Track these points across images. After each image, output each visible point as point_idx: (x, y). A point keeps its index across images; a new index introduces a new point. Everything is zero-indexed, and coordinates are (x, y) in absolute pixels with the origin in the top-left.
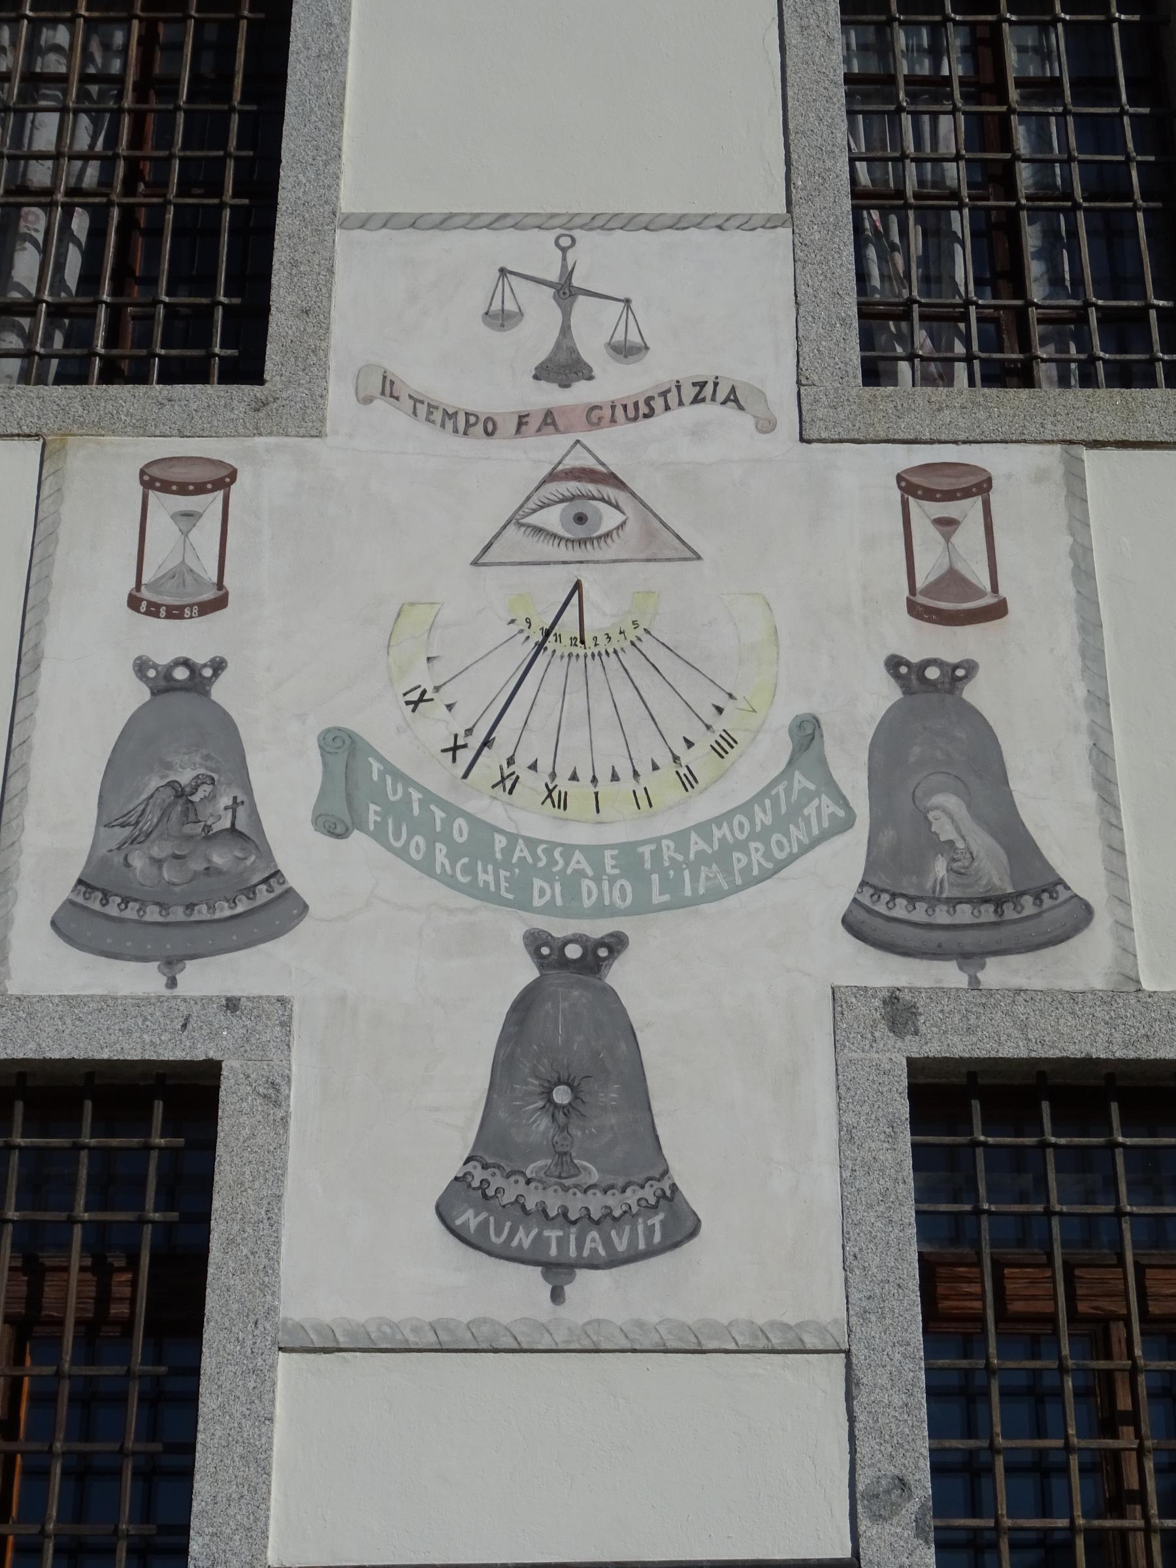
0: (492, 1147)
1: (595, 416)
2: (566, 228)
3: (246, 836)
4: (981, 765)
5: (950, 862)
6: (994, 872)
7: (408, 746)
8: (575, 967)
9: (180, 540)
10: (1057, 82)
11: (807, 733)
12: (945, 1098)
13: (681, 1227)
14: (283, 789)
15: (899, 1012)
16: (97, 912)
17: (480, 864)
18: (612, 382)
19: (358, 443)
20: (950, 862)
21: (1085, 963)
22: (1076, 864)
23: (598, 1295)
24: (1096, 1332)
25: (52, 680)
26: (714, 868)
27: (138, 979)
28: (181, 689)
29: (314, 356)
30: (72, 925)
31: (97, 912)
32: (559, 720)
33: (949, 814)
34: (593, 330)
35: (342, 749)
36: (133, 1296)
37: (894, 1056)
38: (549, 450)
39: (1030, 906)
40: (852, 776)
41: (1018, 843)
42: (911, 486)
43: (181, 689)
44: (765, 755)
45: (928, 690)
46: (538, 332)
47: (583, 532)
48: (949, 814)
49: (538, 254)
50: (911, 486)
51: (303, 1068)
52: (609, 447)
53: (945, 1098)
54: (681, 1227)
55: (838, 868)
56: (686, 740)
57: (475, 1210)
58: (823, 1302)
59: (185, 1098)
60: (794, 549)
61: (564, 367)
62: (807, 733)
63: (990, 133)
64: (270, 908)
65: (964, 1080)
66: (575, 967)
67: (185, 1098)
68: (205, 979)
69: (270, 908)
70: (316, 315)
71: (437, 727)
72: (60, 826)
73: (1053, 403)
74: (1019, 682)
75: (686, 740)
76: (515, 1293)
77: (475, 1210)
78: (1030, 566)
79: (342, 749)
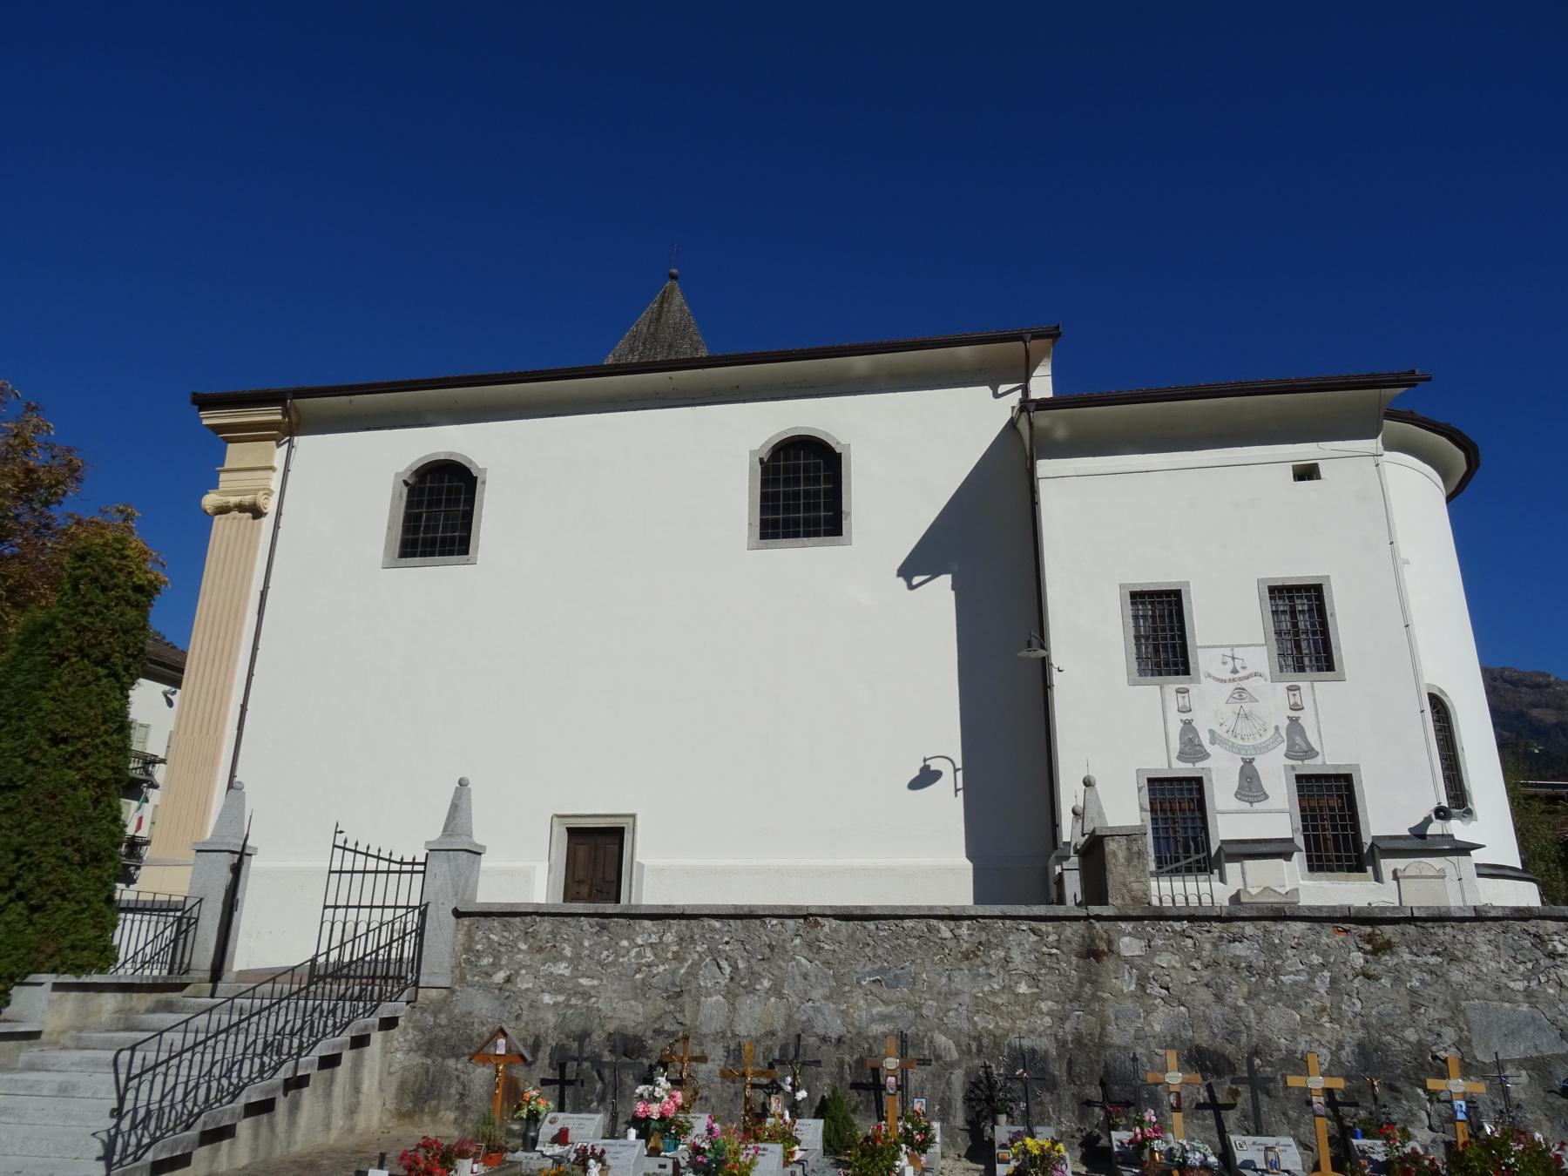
0: (1240, 787)
1: (1241, 679)
2: (1232, 647)
3: (1200, 745)
4: (1302, 732)
5: (1299, 748)
6: (1305, 747)
7: (1220, 731)
8: (1248, 762)
9: (1183, 701)
10: (1103, 901)
11: (1277, 728)
12: (1299, 778)
13: (1267, 797)
14: (1205, 738)
15: (1293, 768)
16: (1182, 756)
17: (1233, 748)
18: (1242, 673)
19: (1206, 683)
20: (1299, 748)
21: (1318, 761)
22: (1316, 746)
23: (1257, 806)
24: (1321, 809)
25: (1169, 723)
26: (1265, 748)
27: (1190, 765)
28: (1188, 724)
29: (1197, 670)
30: (1179, 758)
31: (1182, 756)
32: (1244, 727)
33: (1298, 739)
34: (1238, 664)
35: (1211, 732)
36: (1194, 805)
37: (1293, 774)
38: (1234, 685)
39: (1310, 753)
40: (1284, 734)
41: (1308, 743)
42: (1289, 689)
43: (1188, 724)
44: (1271, 732)
45: (1294, 721)
46: (1230, 666)
47: (1241, 698)
48: (1298, 739)
49: (1228, 652)
50: (1289, 689)
51: (1214, 777)
52: (1243, 684)
53: (1299, 778)
54: (1267, 797)
55: (1283, 747)
56: (916, 784)
57: (1240, 795)
58: (1287, 807)
59: (1199, 780)
60: (1272, 698)
61: (1235, 671)
62: (1277, 728)
63: (1295, 625)
64: (1206, 756)
65: (940, 592)
66: (1248, 762)
67: (1199, 780)
68: (1199, 765)
69: (1206, 756)
70: (1196, 663)
71: (1224, 729)
72: (1175, 745)
73: (1309, 674)
74: (1307, 719)
75: (916, 784)
76: (1246, 806)
77: (1240, 795)
78: (1307, 702)
79: (1211, 732)
